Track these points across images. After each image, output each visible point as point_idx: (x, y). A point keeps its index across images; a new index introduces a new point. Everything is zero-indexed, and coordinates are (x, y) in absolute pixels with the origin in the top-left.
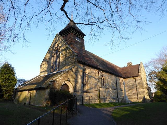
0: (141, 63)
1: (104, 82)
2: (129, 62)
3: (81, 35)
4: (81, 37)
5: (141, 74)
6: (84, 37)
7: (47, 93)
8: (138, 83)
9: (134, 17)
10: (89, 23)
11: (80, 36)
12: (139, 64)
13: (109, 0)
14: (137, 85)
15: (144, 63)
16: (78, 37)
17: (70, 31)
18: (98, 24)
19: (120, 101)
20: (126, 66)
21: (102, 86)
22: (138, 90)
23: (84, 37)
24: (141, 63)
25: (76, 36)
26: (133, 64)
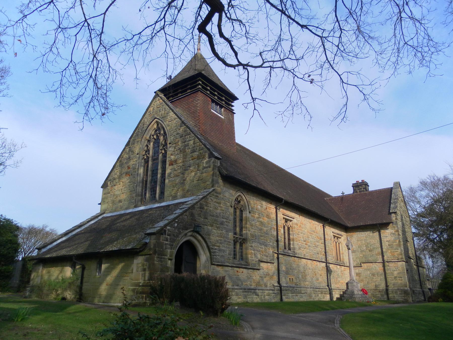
0: (398, 185)
1: (289, 239)
2: (360, 181)
3: (226, 98)
4: (226, 103)
5: (396, 219)
6: (232, 104)
7: (138, 268)
8: (387, 243)
9: (126, 41)
10: (264, 63)
11: (222, 100)
12: (392, 188)
13: (402, 1)
14: (384, 250)
15: (405, 186)
16: (217, 104)
17: (196, 86)
18: (289, 64)
19: (336, 295)
20: (349, 191)
21: (236, 262)
22: (386, 264)
23: (232, 104)
24: (398, 185)
25: (213, 101)
26: (371, 189)
